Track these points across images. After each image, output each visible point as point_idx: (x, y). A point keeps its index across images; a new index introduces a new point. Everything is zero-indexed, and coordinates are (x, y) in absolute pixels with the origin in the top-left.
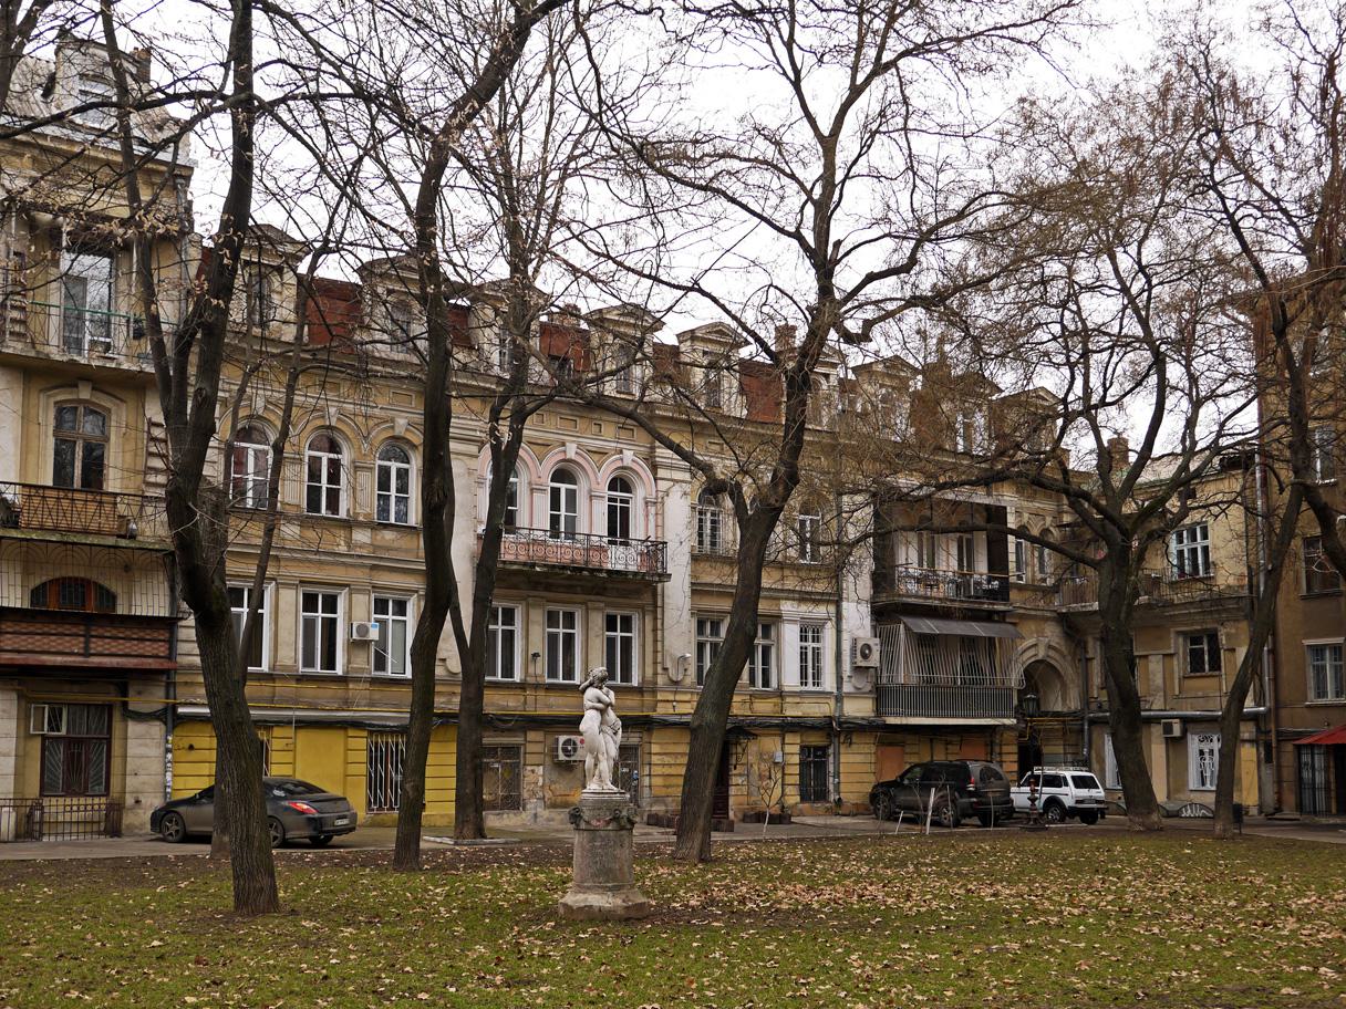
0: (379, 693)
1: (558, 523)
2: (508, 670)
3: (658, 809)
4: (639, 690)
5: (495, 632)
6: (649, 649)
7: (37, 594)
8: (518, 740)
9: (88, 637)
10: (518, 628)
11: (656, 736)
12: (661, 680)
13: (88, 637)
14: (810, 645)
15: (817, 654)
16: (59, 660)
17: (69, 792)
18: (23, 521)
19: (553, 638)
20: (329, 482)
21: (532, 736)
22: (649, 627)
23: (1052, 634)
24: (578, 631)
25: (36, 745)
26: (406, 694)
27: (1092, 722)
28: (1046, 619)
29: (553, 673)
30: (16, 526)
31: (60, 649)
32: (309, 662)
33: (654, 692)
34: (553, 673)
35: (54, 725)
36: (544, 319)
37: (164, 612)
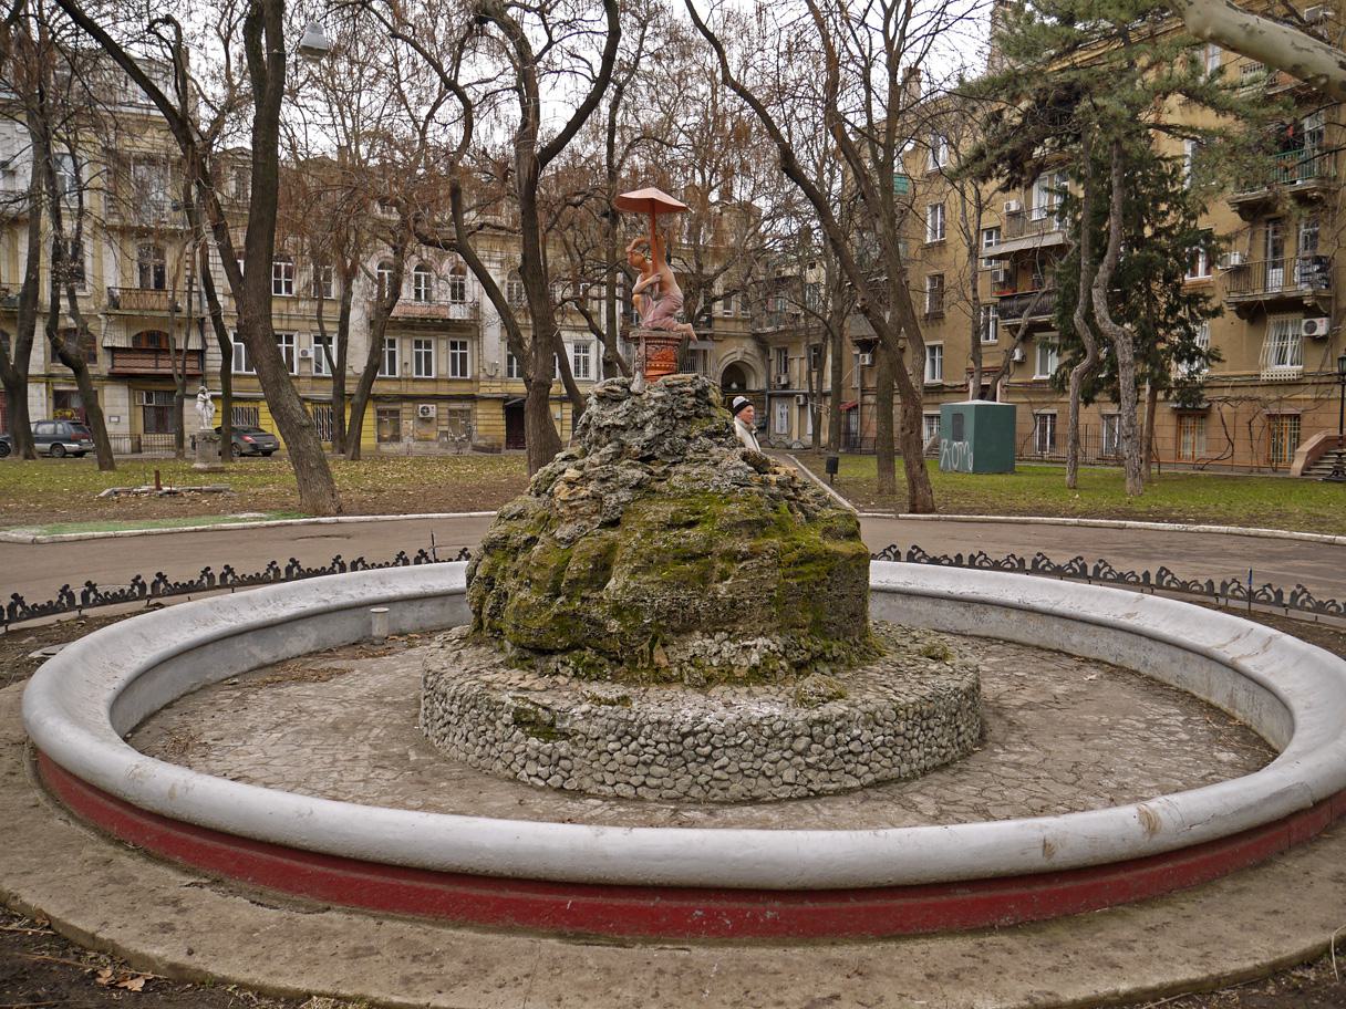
0: (317, 384)
1: (156, 282)
2: (392, 371)
3: (481, 442)
4: (470, 381)
5: (279, 349)
6: (476, 359)
7: (136, 339)
8: (398, 407)
9: (157, 360)
10: (397, 349)
11: (479, 404)
12: (482, 375)
13: (157, 360)
14: (582, 355)
15: (586, 360)
16: (143, 371)
17: (158, 431)
18: (121, 306)
19: (418, 355)
20: (286, 277)
21: (405, 405)
22: (475, 347)
23: (749, 346)
24: (433, 350)
25: (140, 411)
26: (330, 384)
27: (770, 396)
28: (744, 337)
29: (419, 372)
30: (118, 308)
31: (144, 365)
32: (454, 373)
33: (478, 382)
34: (419, 372)
35: (149, 401)
36: (1136, 252)
37: (199, 347)
